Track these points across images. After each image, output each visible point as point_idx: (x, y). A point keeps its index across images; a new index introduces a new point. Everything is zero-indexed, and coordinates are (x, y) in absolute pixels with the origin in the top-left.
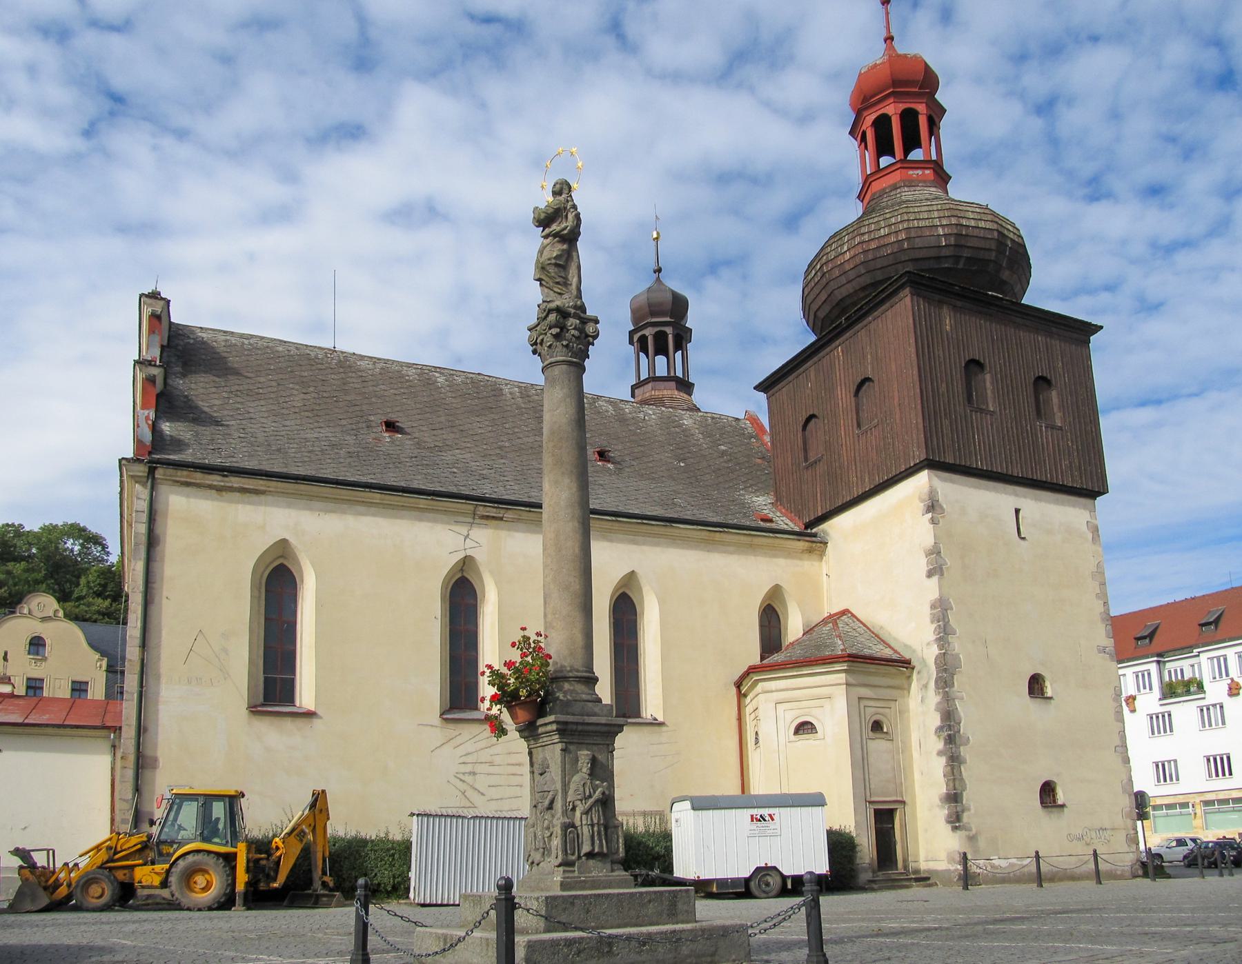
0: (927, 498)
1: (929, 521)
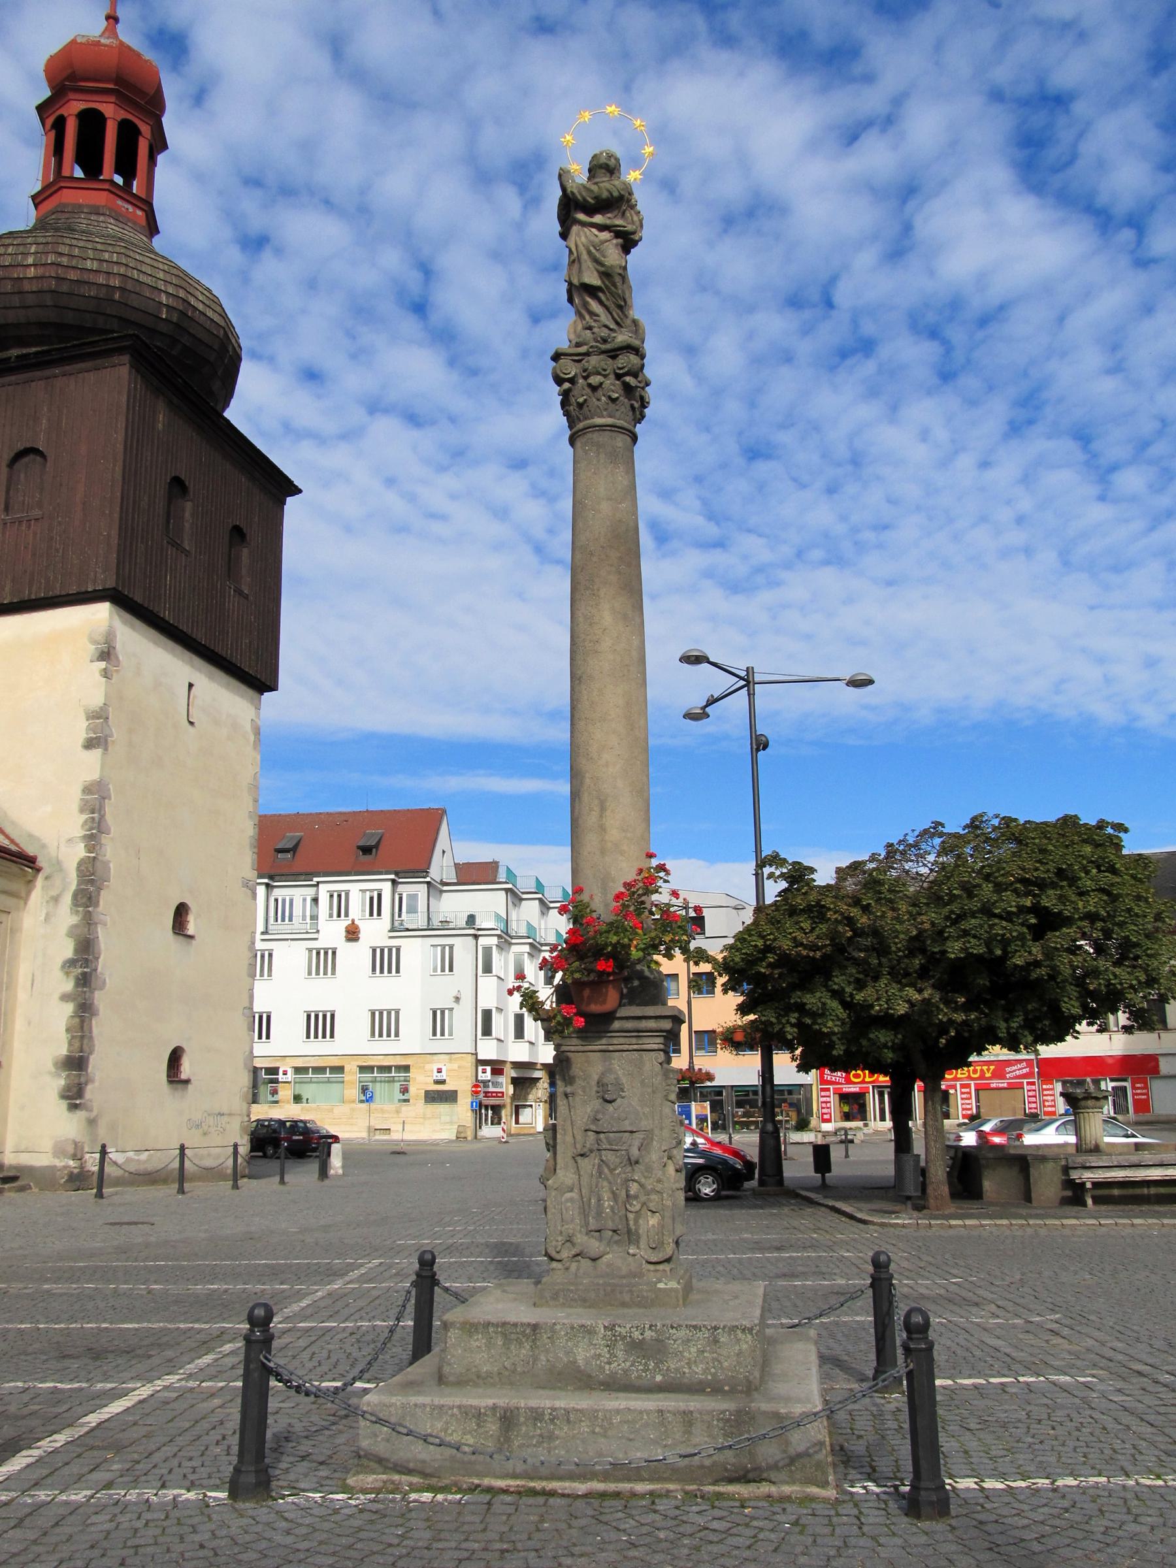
0: (103, 641)
1: (101, 671)
